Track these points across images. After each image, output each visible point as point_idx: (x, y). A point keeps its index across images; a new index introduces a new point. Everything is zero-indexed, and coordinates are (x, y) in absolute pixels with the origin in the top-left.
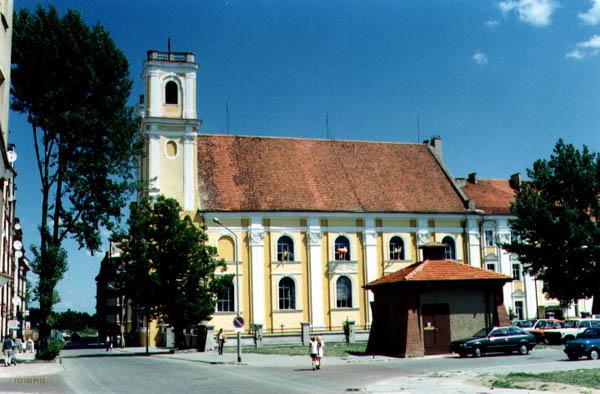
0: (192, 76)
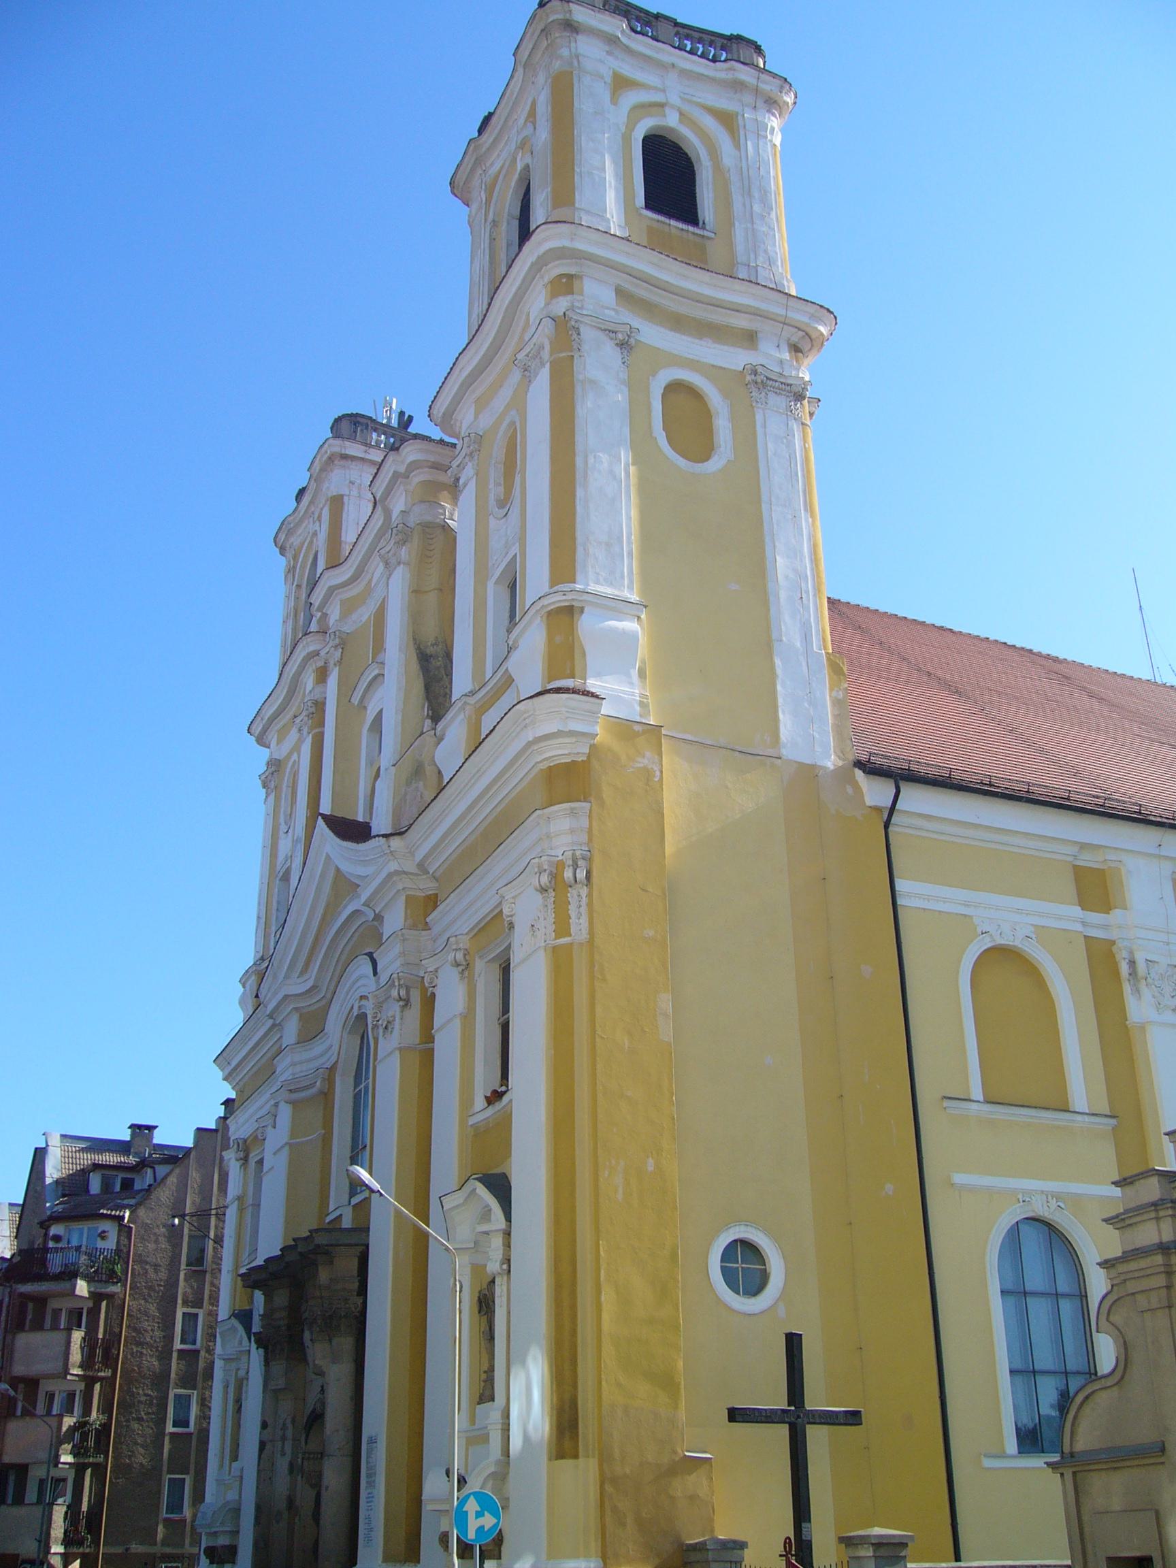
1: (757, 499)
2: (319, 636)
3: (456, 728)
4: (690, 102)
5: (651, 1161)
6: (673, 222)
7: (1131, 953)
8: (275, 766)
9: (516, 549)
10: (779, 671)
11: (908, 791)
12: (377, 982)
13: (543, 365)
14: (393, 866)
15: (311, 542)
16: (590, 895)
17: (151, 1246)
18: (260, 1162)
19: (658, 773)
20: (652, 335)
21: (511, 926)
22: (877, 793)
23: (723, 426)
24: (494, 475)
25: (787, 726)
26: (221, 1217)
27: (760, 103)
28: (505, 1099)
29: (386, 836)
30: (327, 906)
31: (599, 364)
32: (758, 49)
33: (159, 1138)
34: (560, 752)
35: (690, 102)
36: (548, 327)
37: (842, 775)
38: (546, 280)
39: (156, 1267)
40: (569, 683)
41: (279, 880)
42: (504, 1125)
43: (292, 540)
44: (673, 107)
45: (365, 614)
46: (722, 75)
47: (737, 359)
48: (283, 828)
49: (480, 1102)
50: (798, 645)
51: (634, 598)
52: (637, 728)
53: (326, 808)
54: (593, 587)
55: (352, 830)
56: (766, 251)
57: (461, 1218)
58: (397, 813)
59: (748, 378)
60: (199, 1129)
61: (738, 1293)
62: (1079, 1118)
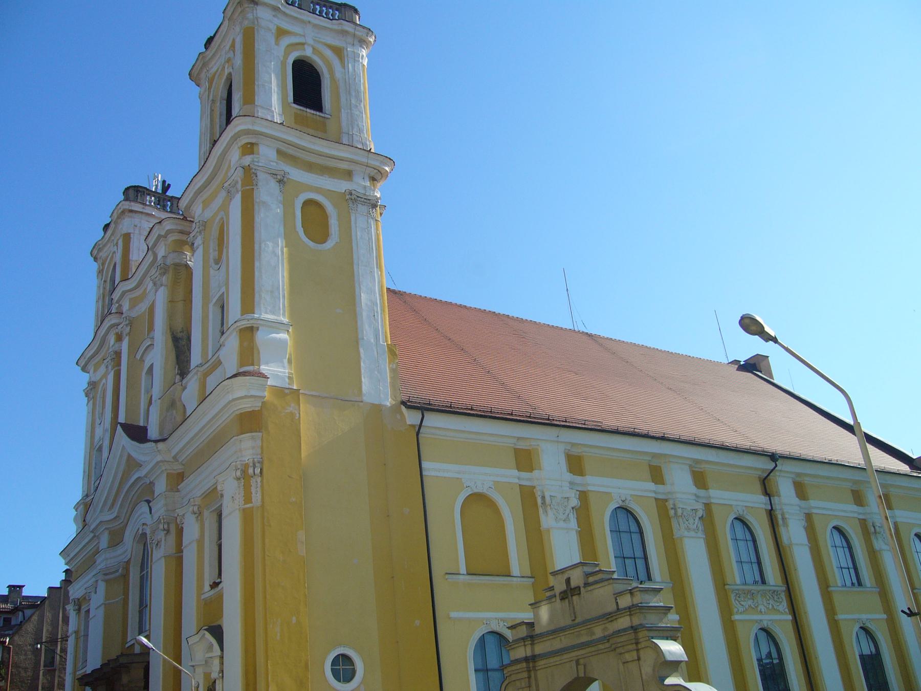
1: (351, 264)
2: (117, 315)
3: (192, 383)
4: (319, 42)
5: (294, 618)
6: (308, 110)
7: (543, 492)
8: (93, 385)
9: (223, 289)
10: (362, 355)
11: (427, 415)
12: (152, 517)
13: (238, 192)
14: (159, 458)
15: (112, 257)
16: (262, 481)
17: (22, 657)
18: (88, 611)
20: (297, 175)
21: (222, 496)
22: (412, 418)
23: (334, 223)
24: (213, 245)
25: (366, 385)
26: (65, 639)
27: (356, 42)
28: (220, 586)
29: (156, 441)
30: (123, 475)
31: (268, 193)
32: (356, 11)
33: (26, 592)
34: (247, 406)
35: (319, 42)
36: (240, 173)
37: (395, 409)
38: (240, 144)
39: (26, 669)
40: (250, 368)
41: (95, 451)
42: (220, 597)
43: (101, 254)
44: (309, 45)
45: (143, 307)
46: (335, 27)
47: (342, 186)
48: (98, 421)
49: (207, 587)
50: (372, 340)
51: (285, 320)
52: (287, 391)
53: (122, 419)
54: (265, 316)
55: (138, 433)
56: (358, 125)
57: (199, 647)
58: (161, 433)
59: (347, 197)
60: (50, 588)
61: (339, 681)
62: (515, 579)
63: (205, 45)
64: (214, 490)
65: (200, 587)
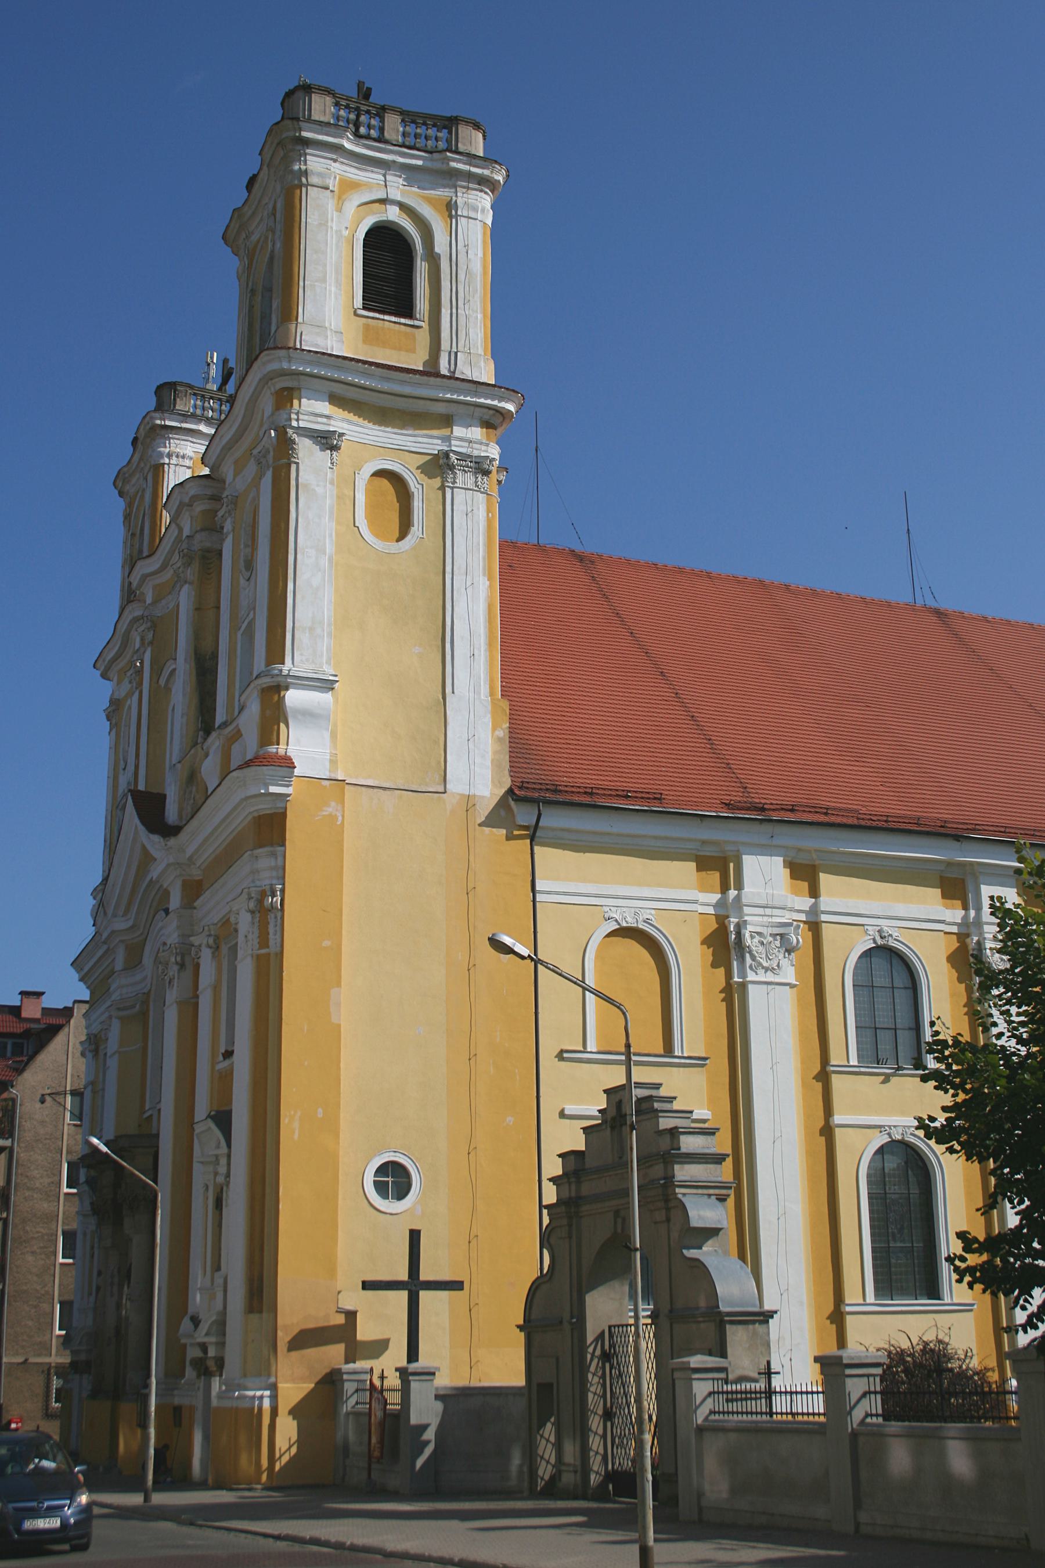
0: (479, 207)
5: (320, 1110)
19: (340, 818)
57: (207, 1132)
63: (247, 187)
64: (226, 922)
65: (214, 1055)
